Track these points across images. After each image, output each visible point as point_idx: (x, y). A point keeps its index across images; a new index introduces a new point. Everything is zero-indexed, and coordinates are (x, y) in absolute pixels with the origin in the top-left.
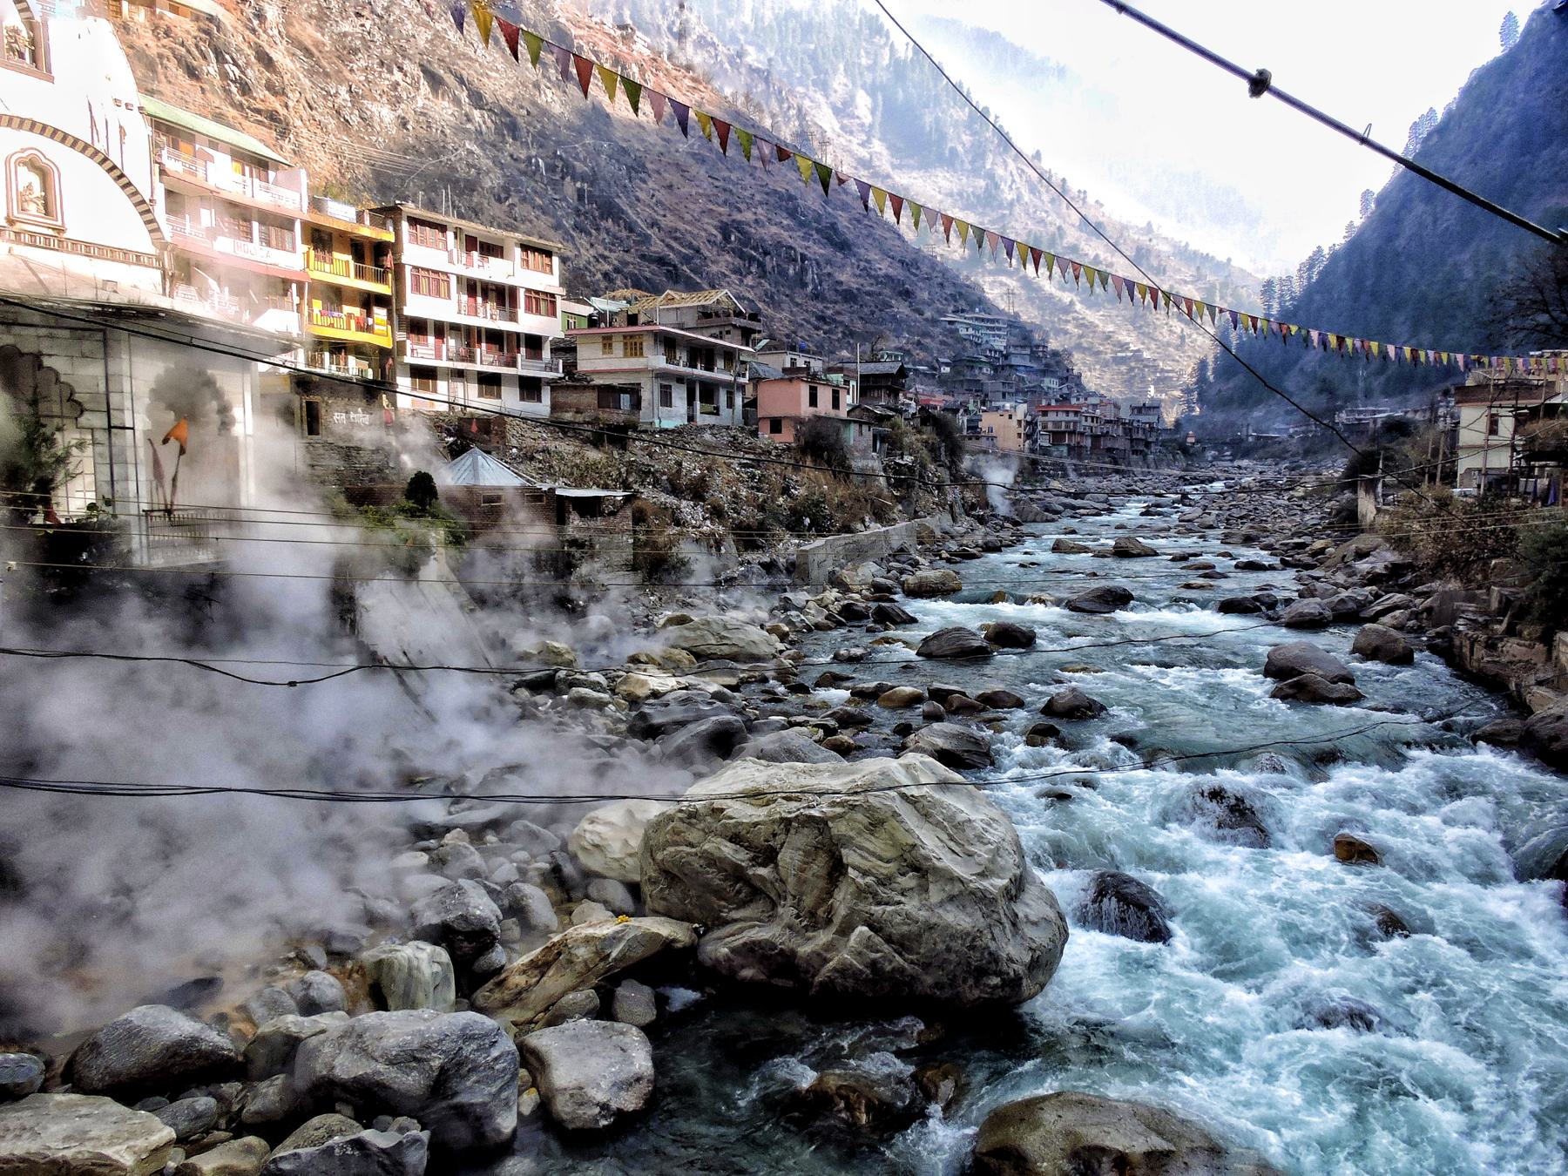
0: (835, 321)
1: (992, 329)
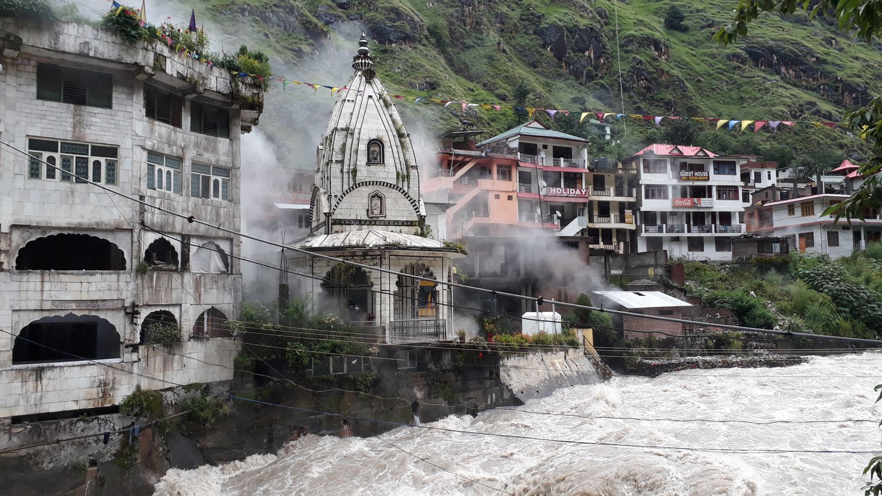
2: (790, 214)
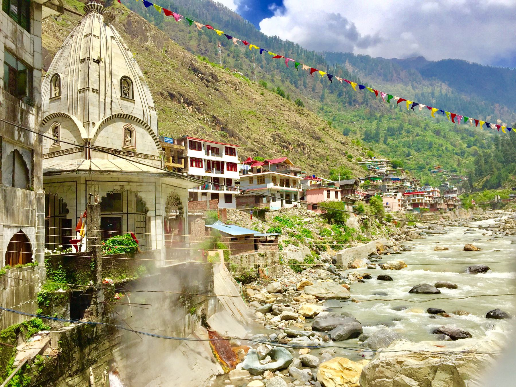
0: (317, 167)
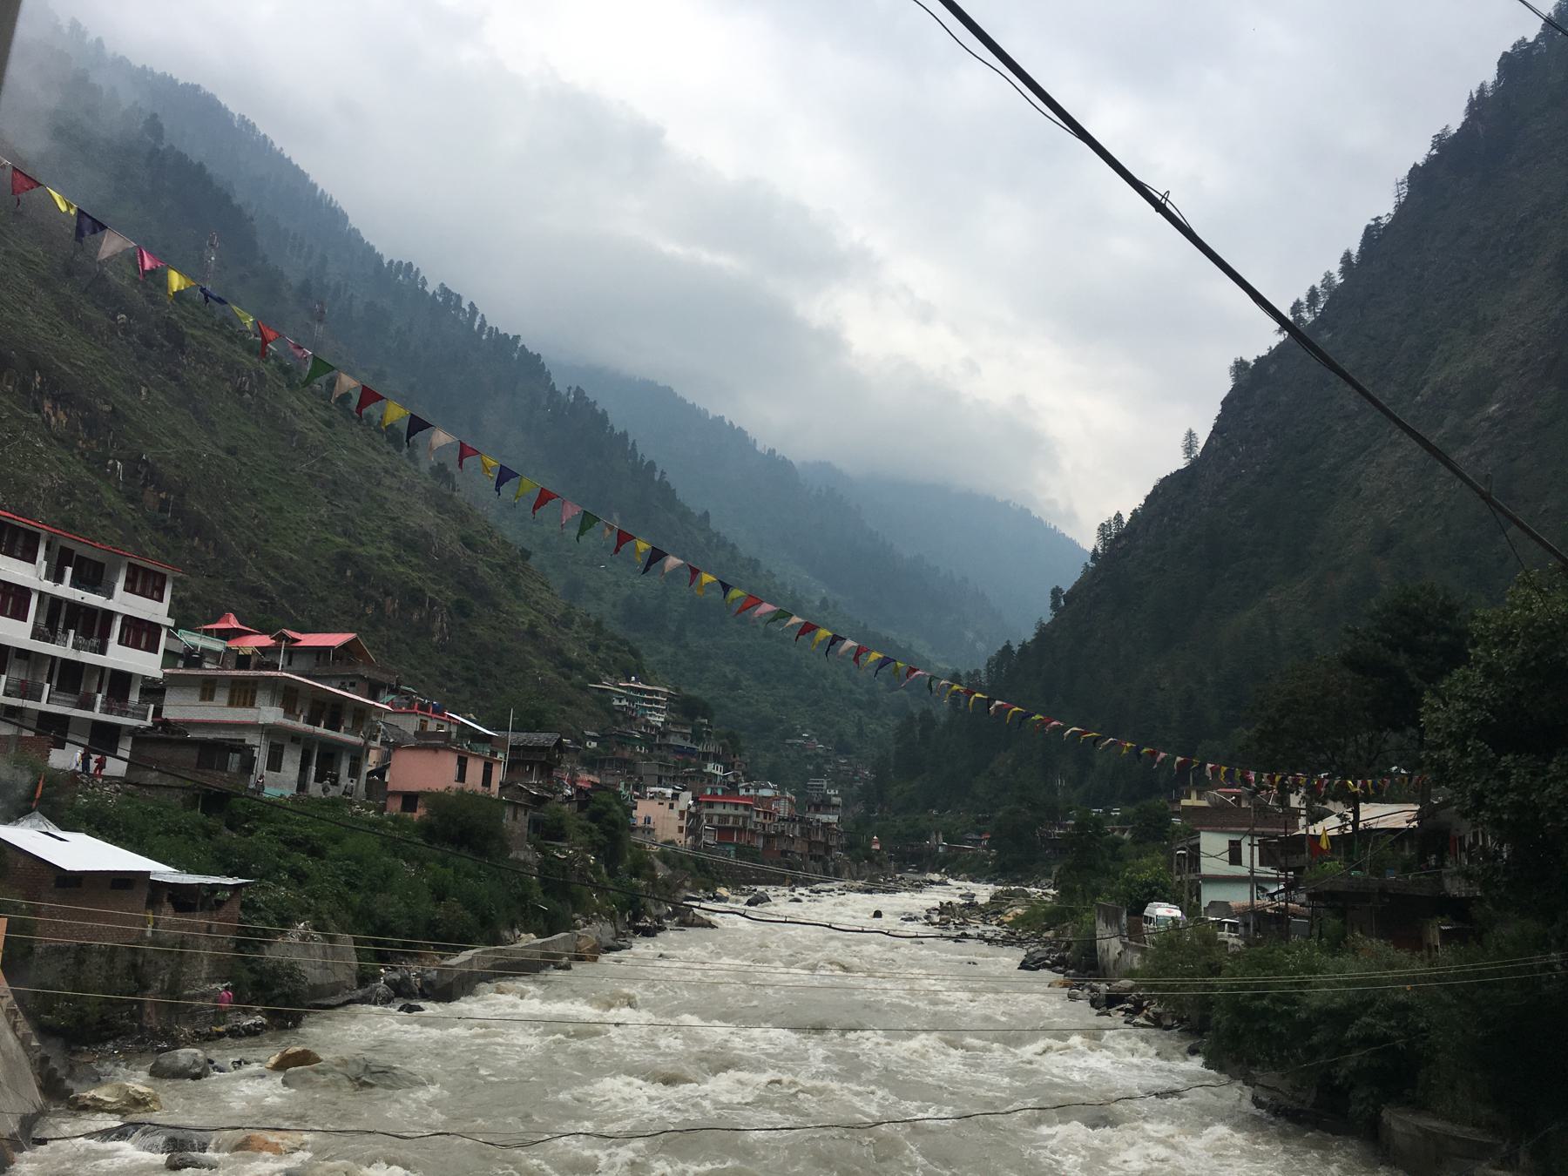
1: (650, 701)
2: (203, 698)
